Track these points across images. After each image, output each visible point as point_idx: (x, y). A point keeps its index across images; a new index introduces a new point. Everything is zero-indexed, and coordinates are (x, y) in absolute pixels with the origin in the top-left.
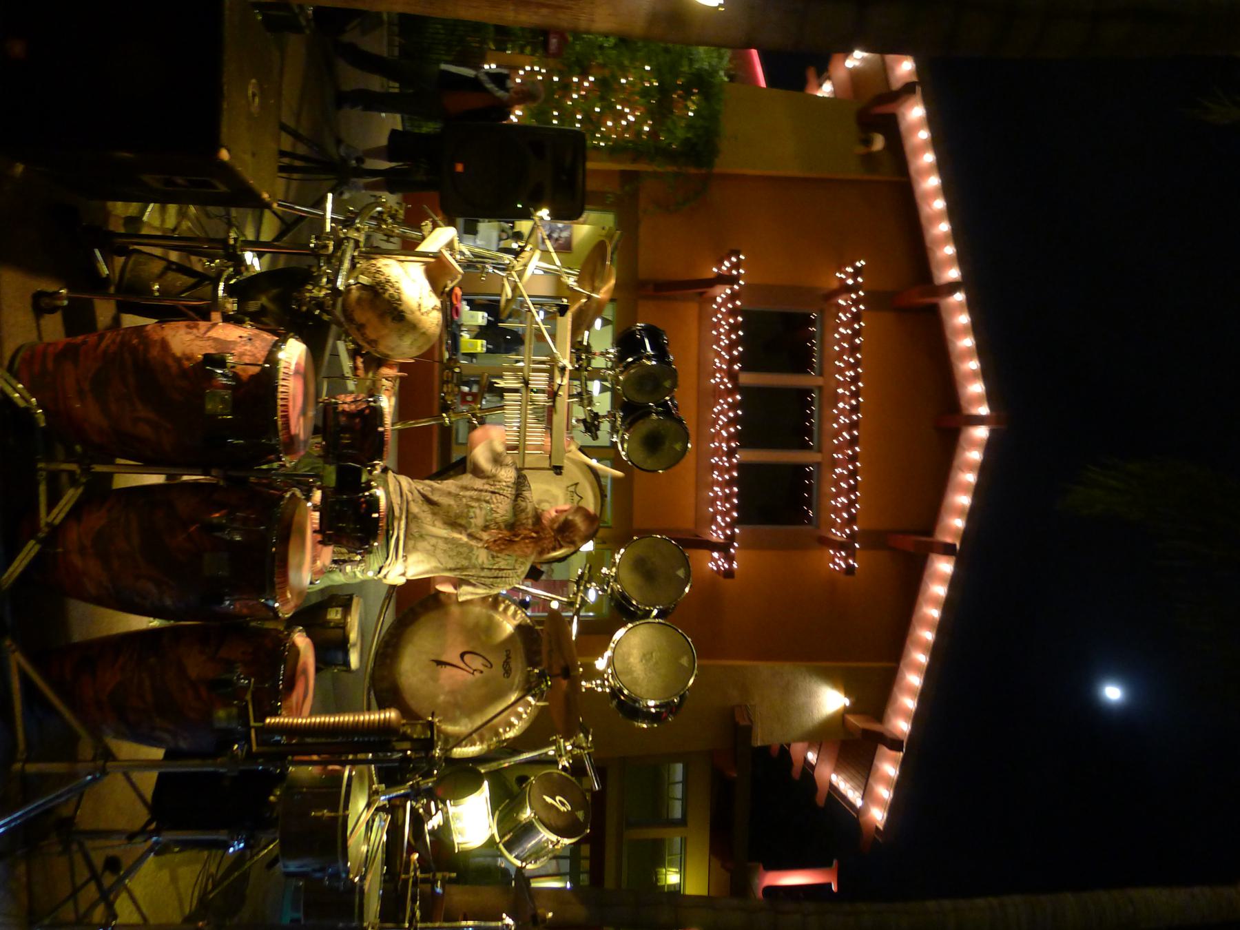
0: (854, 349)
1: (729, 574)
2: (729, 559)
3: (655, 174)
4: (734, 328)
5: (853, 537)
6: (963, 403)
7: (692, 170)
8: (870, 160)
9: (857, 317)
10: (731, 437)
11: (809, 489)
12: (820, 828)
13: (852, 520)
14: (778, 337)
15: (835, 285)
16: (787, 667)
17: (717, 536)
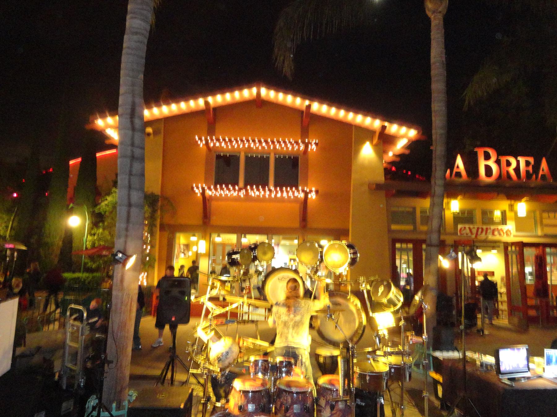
0: (230, 141)
1: (317, 192)
2: (311, 191)
3: (162, 218)
4: (222, 189)
5: (303, 142)
6: (251, 98)
7: (160, 204)
8: (156, 133)
9: (218, 140)
10: (264, 189)
11: (285, 157)
12: (418, 153)
13: (297, 143)
14: (225, 168)
15: (205, 147)
16: (354, 168)
17: (302, 195)
